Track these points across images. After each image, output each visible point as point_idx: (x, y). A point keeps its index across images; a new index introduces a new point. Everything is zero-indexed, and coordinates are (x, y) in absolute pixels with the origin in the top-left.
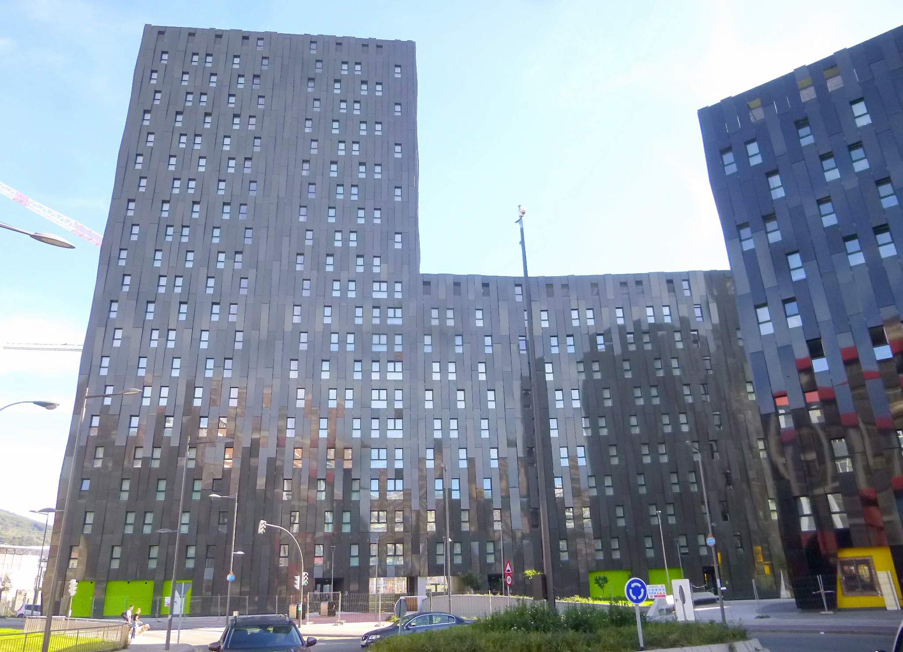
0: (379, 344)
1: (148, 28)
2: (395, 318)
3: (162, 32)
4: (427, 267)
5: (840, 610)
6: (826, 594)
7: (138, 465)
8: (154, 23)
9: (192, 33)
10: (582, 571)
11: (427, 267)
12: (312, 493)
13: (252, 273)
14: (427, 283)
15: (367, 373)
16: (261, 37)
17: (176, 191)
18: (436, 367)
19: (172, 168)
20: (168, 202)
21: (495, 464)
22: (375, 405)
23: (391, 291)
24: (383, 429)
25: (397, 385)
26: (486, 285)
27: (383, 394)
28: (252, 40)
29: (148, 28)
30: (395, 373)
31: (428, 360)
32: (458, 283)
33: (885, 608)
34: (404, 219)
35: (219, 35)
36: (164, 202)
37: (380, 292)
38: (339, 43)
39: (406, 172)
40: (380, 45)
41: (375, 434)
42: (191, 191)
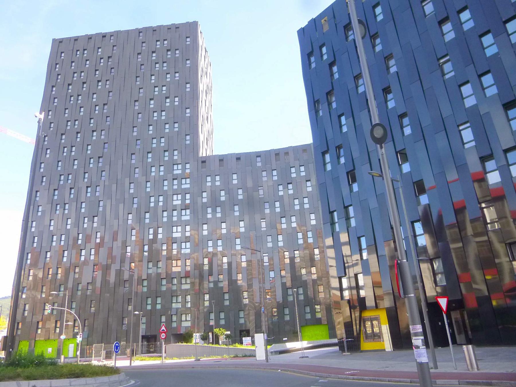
0: (177, 201)
1: (54, 40)
2: (186, 184)
3: (61, 41)
4: (203, 153)
5: (362, 352)
6: (347, 341)
7: (212, 285)
8: (57, 37)
9: (76, 39)
10: (336, 324)
11: (203, 153)
12: (140, 287)
13: (107, 168)
14: (204, 162)
15: (170, 217)
16: (112, 35)
17: (154, 146)
18: (209, 210)
19: (151, 132)
20: (150, 152)
21: (244, 264)
22: (175, 235)
23: (184, 169)
24: (180, 248)
25: (187, 223)
26: (238, 159)
27: (179, 229)
28: (108, 37)
29: (54, 40)
30: (186, 216)
31: (205, 207)
32: (222, 159)
33: (384, 350)
34: (192, 127)
35: (90, 38)
36: (148, 153)
37: (178, 171)
38: (154, 30)
39: (192, 100)
40: (177, 27)
41: (175, 252)
42: (162, 145)
